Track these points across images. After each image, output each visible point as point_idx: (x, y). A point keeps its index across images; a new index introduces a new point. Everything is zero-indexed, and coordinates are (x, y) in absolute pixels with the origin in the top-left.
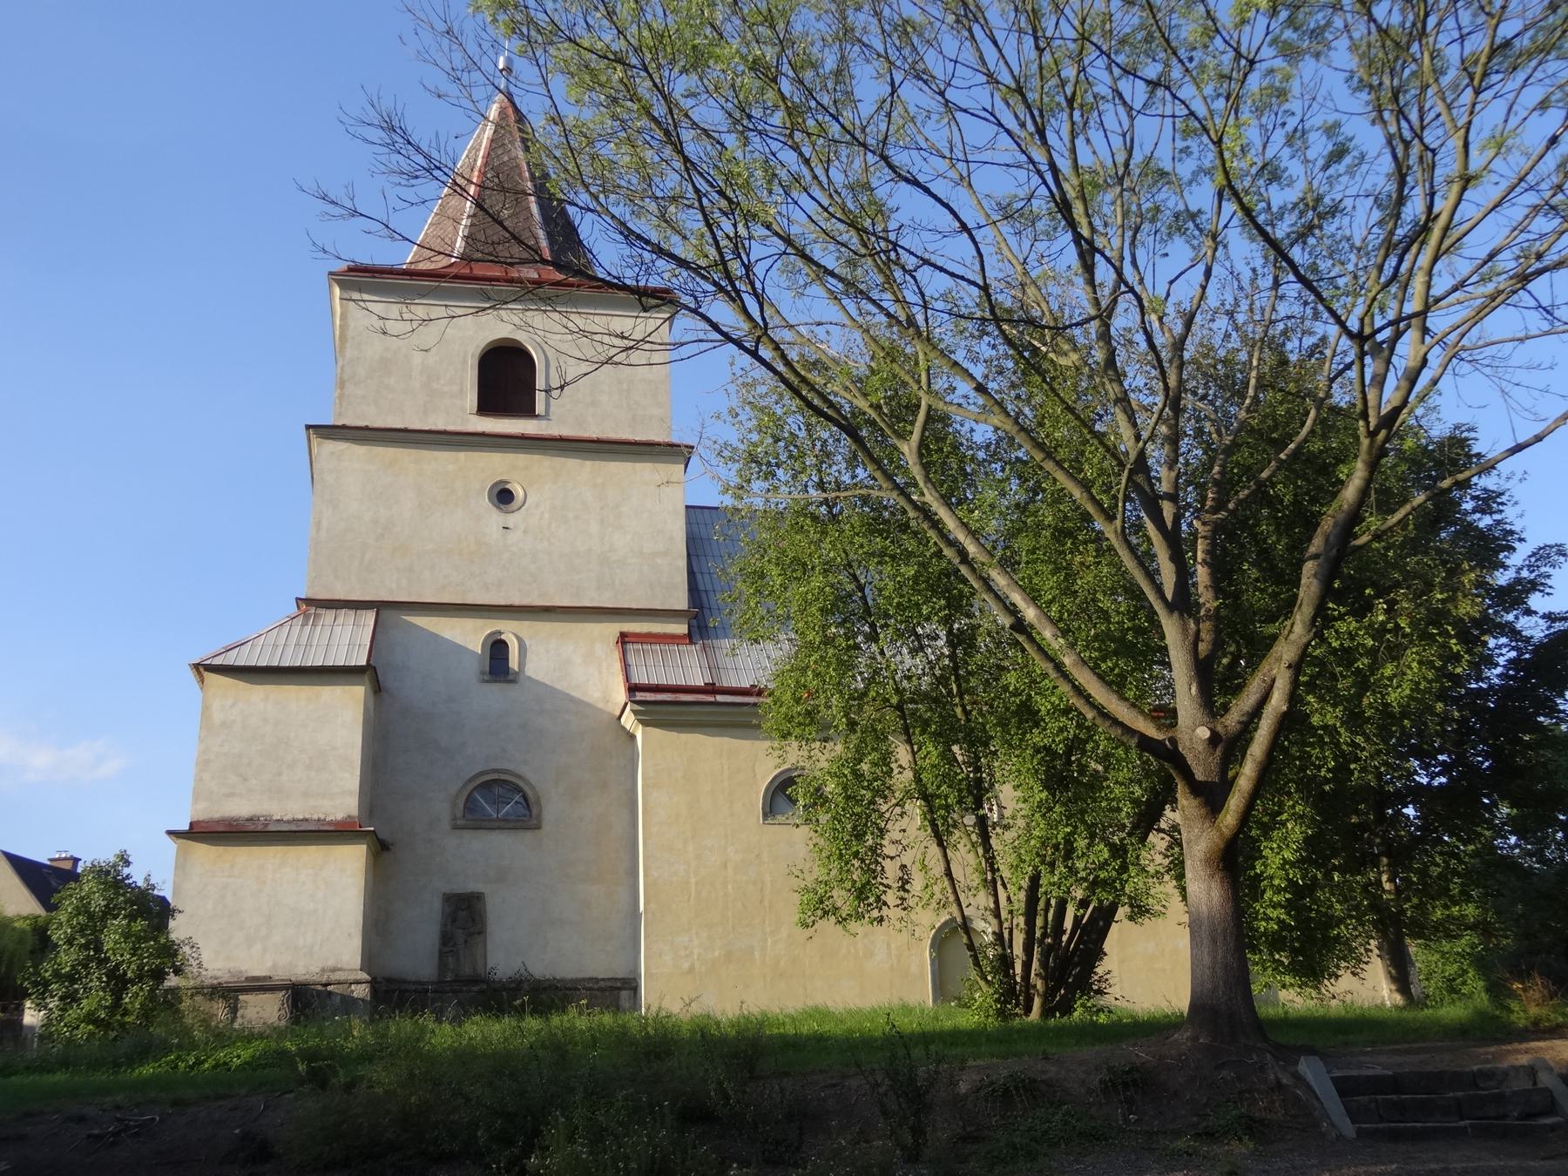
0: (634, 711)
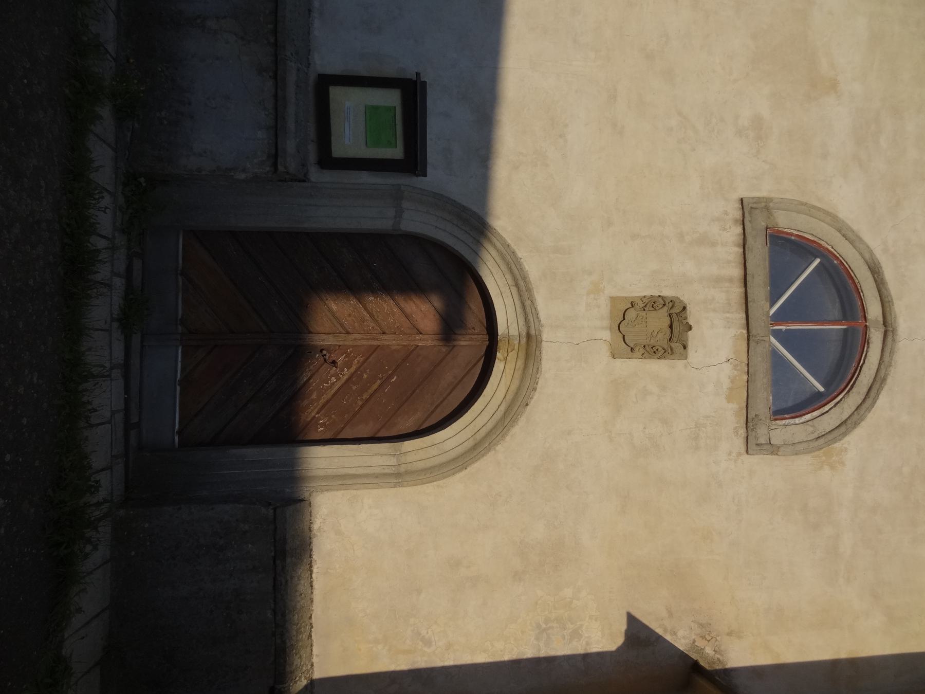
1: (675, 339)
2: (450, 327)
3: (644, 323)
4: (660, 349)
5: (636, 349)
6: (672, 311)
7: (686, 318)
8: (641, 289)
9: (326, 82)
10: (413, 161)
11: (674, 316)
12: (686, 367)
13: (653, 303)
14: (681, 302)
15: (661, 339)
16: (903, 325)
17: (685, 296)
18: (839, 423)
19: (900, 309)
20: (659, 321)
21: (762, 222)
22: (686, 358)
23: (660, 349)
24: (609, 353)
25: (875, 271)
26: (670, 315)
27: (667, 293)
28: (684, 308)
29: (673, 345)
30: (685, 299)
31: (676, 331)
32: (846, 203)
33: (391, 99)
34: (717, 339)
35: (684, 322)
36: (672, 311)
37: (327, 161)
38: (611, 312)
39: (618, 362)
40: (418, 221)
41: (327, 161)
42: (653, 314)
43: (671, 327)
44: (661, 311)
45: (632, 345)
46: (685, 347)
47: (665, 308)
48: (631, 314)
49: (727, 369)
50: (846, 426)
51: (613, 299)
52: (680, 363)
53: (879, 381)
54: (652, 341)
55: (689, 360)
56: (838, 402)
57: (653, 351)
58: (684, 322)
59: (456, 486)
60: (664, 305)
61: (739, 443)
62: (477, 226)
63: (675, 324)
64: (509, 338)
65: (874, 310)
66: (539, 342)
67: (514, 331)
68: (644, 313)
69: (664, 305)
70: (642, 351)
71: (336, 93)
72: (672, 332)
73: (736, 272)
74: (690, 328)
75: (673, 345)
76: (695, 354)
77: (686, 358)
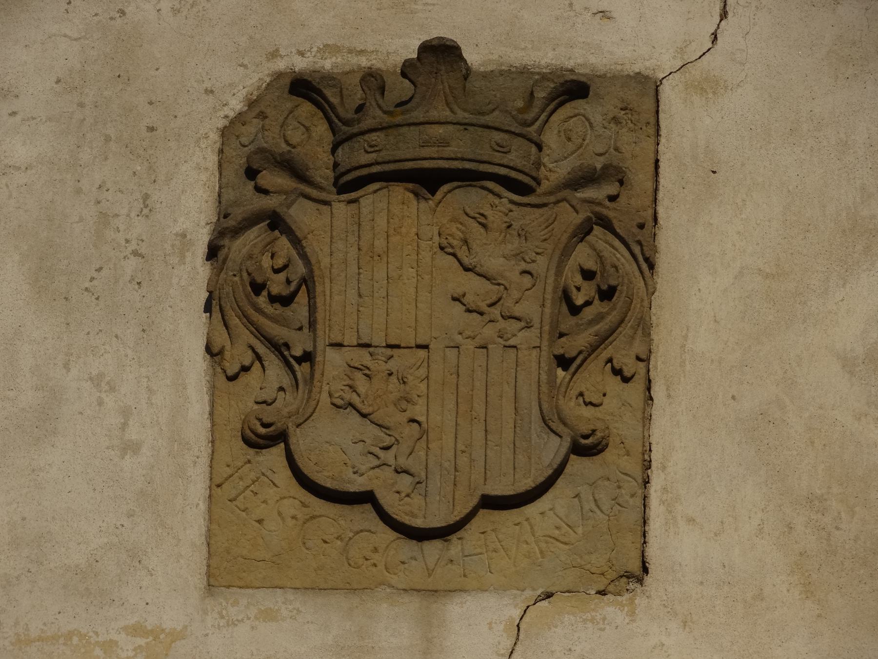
1: (517, 155)
3: (401, 361)
4: (583, 256)
5: (583, 417)
6: (323, 174)
7: (373, 80)
8: (156, 382)
11: (357, 156)
12: (709, 87)
13: (261, 300)
14: (255, 104)
15: (510, 245)
17: (218, 77)
18: (433, 126)
20: (387, 266)
22: (649, 87)
23: (583, 256)
24: (611, 610)
26: (350, 184)
27: (191, 198)
28: (302, 87)
29: (557, 168)
30: (237, 82)
31: (460, 148)
35: (402, 88)
36: (320, 160)
38: (315, 588)
39: (674, 545)
42: (336, 297)
43: (428, 181)
44: (318, 249)
45: (552, 449)
46: (574, 89)
47: (303, 215)
48: (334, 445)
51: (226, 571)
52: (687, 125)
54: (528, 308)
55: (659, 59)
56: (396, 161)
57: (600, 301)
58: (402, 88)
60: (276, 222)
63: (409, 148)
68: (333, 362)
69: (276, 222)
70: (593, 378)
72: (468, 177)
74: (441, 53)
75: (557, 168)
77: (649, 87)
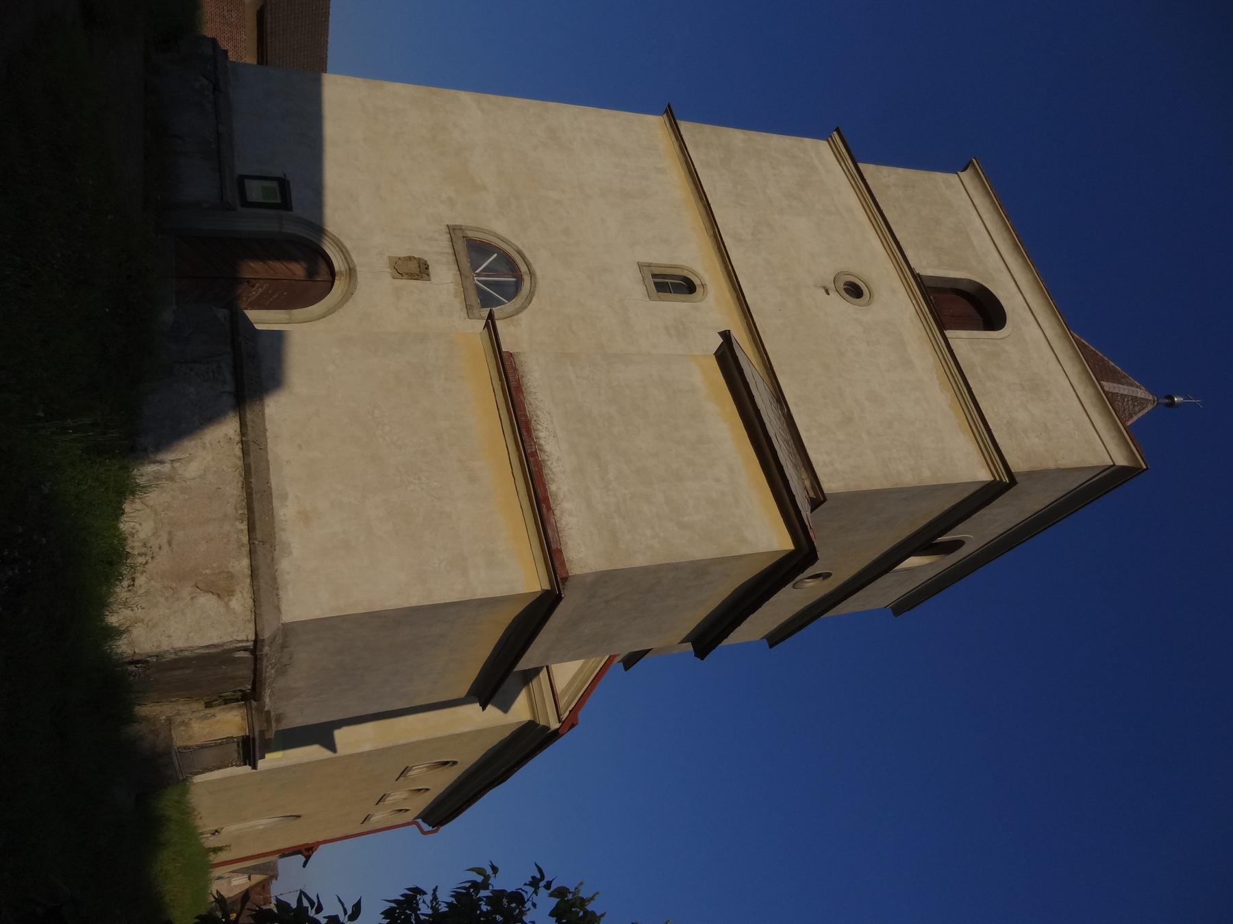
0: (547, 728)
2: (311, 274)
9: (242, 179)
10: (286, 205)
15: (416, 271)
16: (539, 273)
19: (535, 267)
20: (413, 267)
21: (460, 234)
25: (520, 253)
32: (499, 227)
33: (275, 184)
34: (445, 277)
37: (246, 203)
40: (290, 229)
41: (246, 203)
49: (541, 435)
50: (519, 311)
51: (390, 258)
53: (532, 294)
57: (412, 276)
59: (320, 324)
61: (464, 314)
62: (320, 230)
64: (341, 272)
65: (523, 268)
66: (355, 271)
67: (343, 269)
71: (248, 183)
73: (451, 251)
76: (434, 279)
